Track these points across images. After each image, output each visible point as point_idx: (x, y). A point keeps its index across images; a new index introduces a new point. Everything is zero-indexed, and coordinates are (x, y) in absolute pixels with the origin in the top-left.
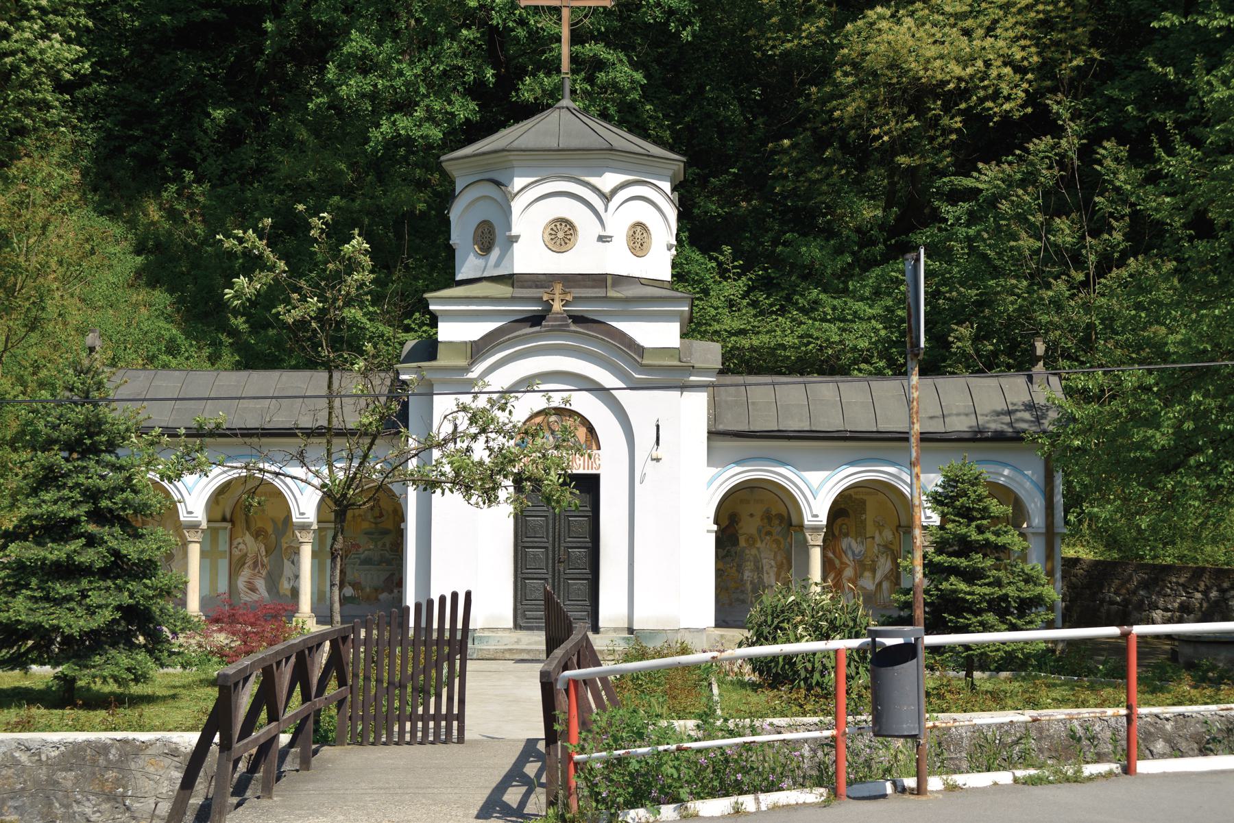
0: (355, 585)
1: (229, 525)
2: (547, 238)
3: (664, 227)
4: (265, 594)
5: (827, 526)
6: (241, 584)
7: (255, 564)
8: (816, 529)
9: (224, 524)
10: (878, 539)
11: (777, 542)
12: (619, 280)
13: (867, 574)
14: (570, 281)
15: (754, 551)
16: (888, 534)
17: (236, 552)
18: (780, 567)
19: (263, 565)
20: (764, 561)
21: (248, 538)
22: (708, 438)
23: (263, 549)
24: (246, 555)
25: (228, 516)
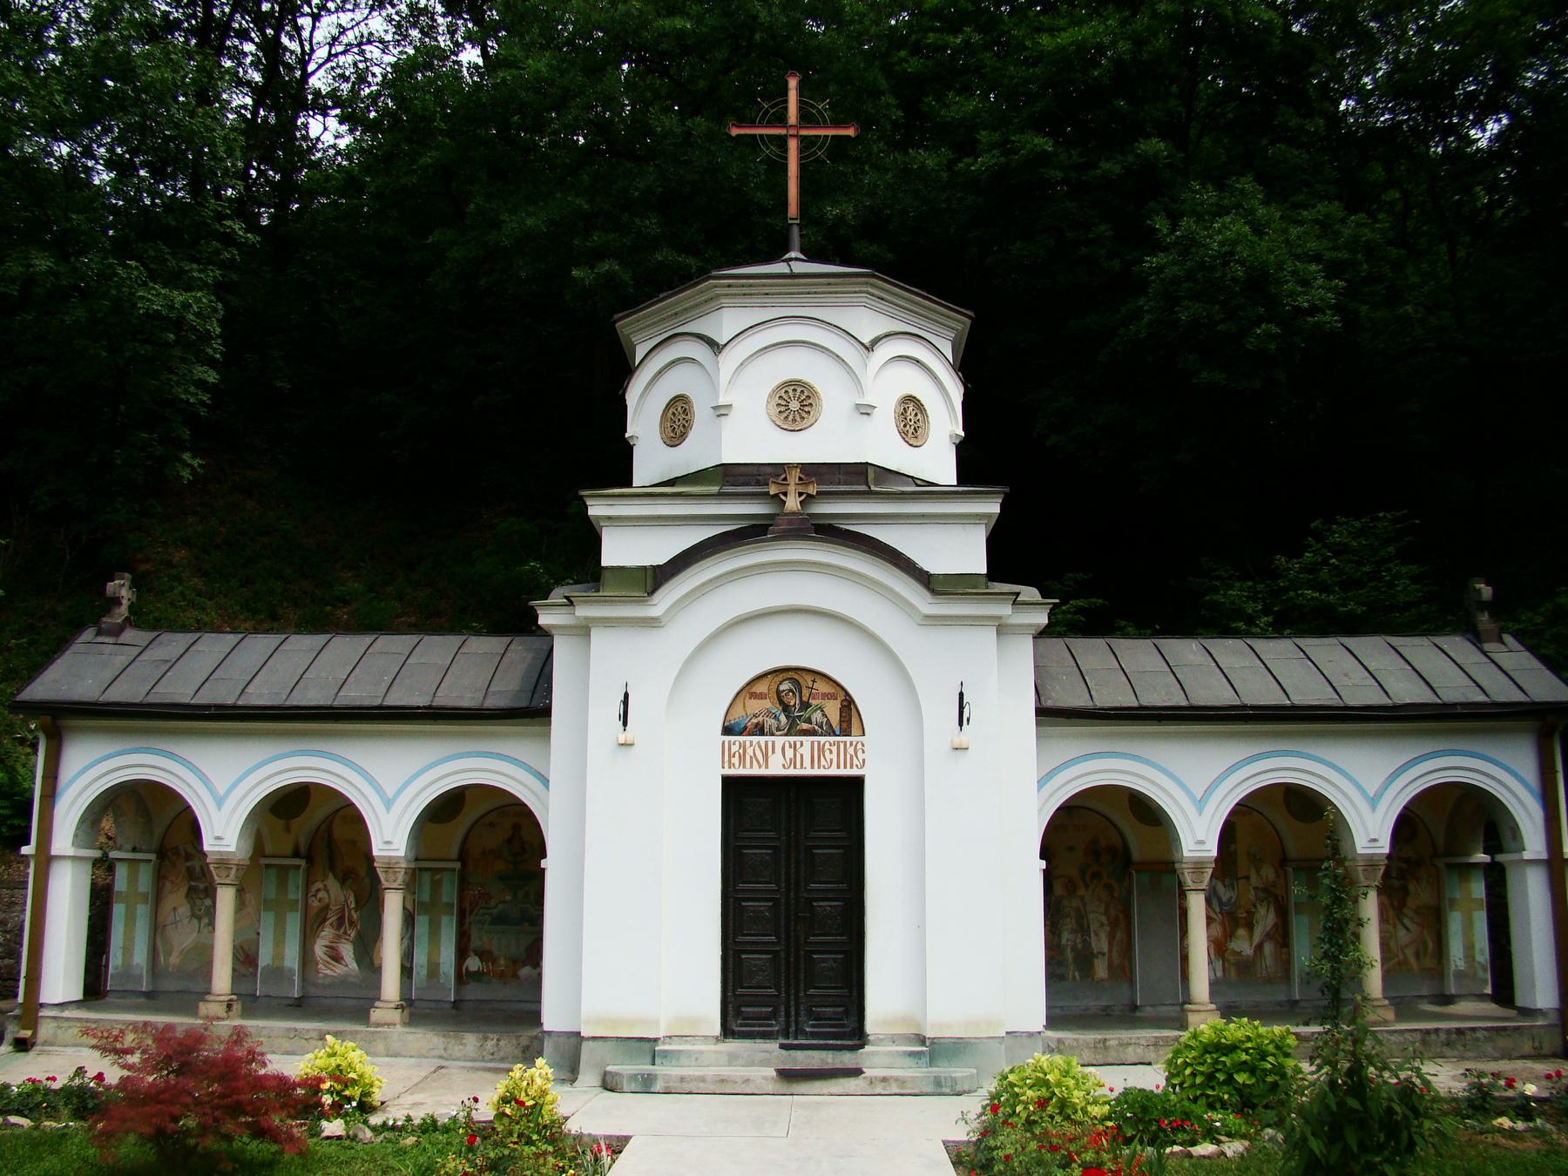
0: (482, 955)
1: (302, 863)
2: (775, 410)
3: (946, 420)
4: (355, 965)
5: (1217, 860)
6: (319, 949)
7: (340, 922)
8: (1198, 866)
9: (296, 862)
10: (1254, 880)
11: (1109, 887)
12: (885, 473)
13: (1241, 932)
14: (812, 471)
15: (1075, 903)
16: (1268, 873)
17: (315, 903)
18: (1114, 924)
19: (352, 923)
20: (1091, 916)
21: (332, 883)
22: (1038, 724)
23: (352, 899)
24: (327, 907)
25: (303, 849)
